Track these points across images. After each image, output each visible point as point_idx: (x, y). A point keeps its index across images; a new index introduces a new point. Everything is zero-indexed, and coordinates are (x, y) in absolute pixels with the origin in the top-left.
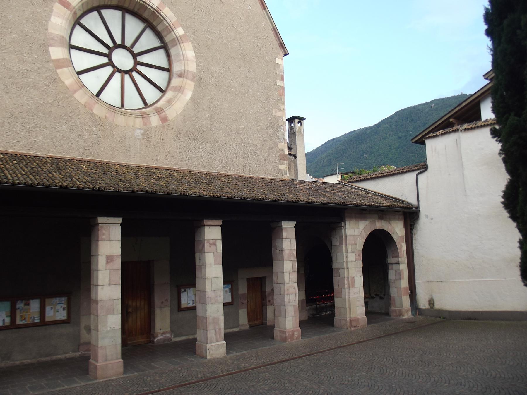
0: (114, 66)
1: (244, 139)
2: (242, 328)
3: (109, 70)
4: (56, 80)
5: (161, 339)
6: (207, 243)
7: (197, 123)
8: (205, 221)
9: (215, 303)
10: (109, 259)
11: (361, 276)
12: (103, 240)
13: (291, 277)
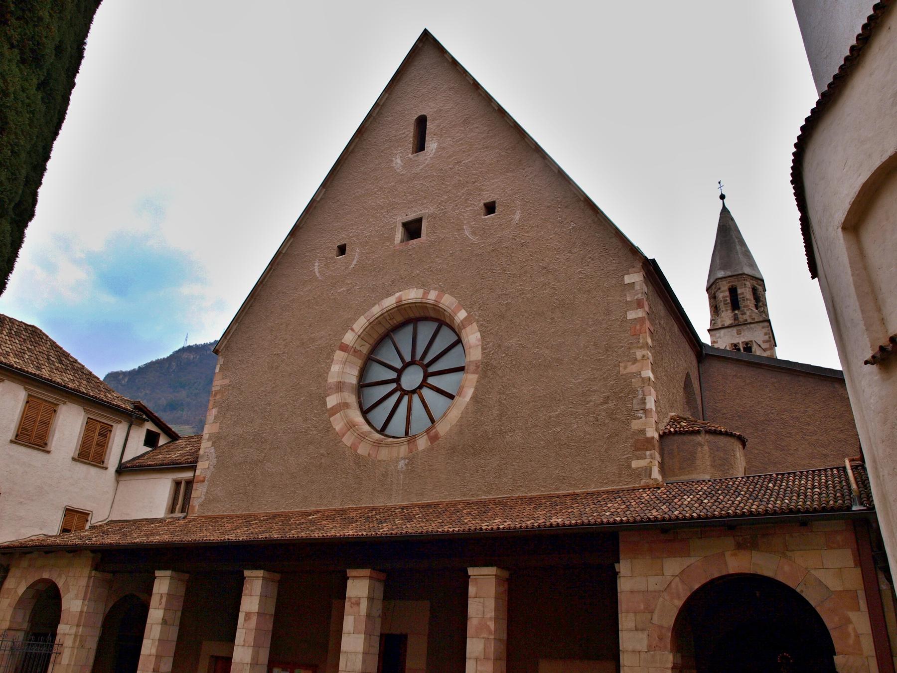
1: (558, 433)
4: (329, 428)
6: (348, 601)
7: (479, 429)
13: (479, 668)
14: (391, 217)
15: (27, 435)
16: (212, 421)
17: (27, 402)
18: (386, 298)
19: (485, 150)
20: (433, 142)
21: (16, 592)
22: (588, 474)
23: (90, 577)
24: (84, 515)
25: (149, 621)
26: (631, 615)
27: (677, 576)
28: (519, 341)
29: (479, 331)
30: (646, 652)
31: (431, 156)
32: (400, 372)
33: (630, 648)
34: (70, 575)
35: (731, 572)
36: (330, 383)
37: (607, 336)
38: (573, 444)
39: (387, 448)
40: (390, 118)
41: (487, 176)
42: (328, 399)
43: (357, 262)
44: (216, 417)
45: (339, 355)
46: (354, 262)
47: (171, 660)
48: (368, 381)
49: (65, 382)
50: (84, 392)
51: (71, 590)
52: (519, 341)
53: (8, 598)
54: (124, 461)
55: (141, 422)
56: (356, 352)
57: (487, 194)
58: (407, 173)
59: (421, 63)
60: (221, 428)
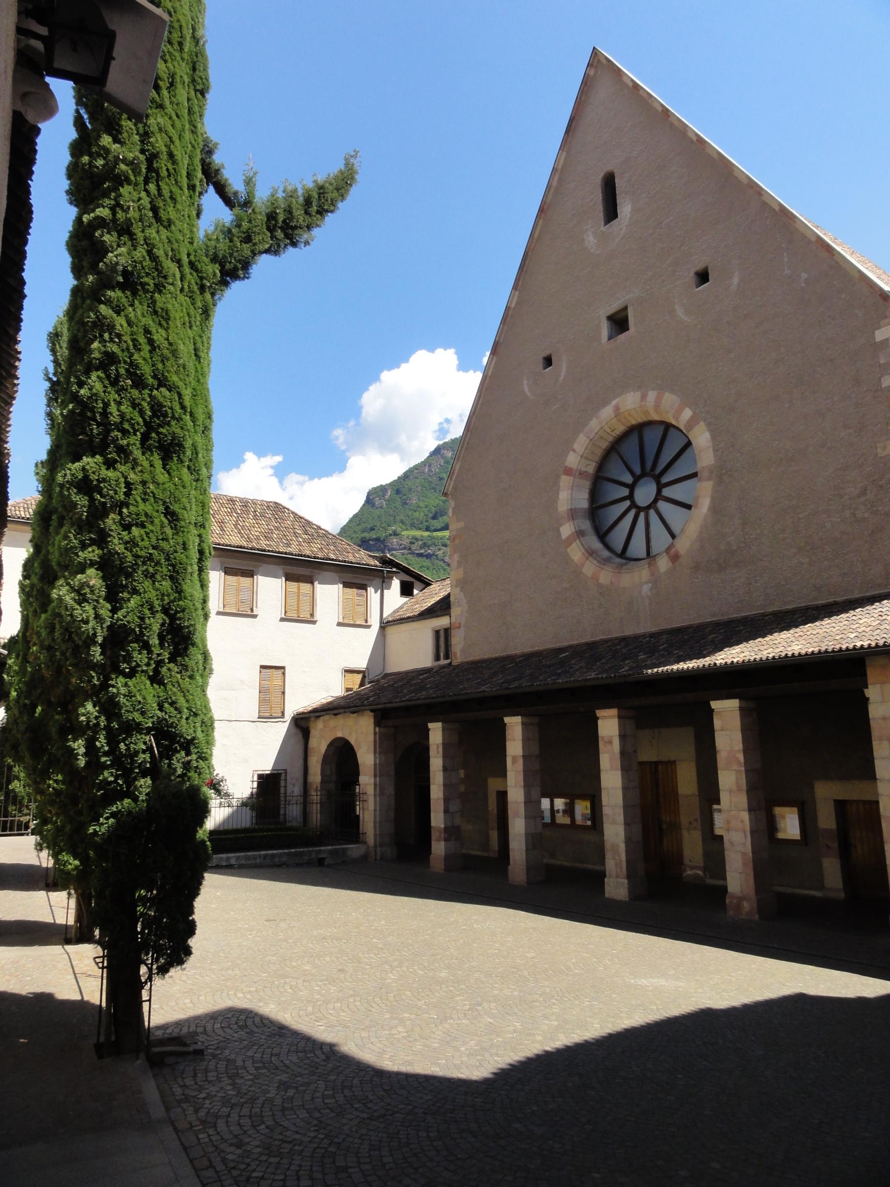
0: (655, 501)
3: (662, 505)
10: (514, 759)
25: (431, 769)
31: (626, 223)
42: (562, 529)
45: (565, 480)
46: (563, 373)
54: (385, 616)
56: (582, 474)
60: (465, 573)
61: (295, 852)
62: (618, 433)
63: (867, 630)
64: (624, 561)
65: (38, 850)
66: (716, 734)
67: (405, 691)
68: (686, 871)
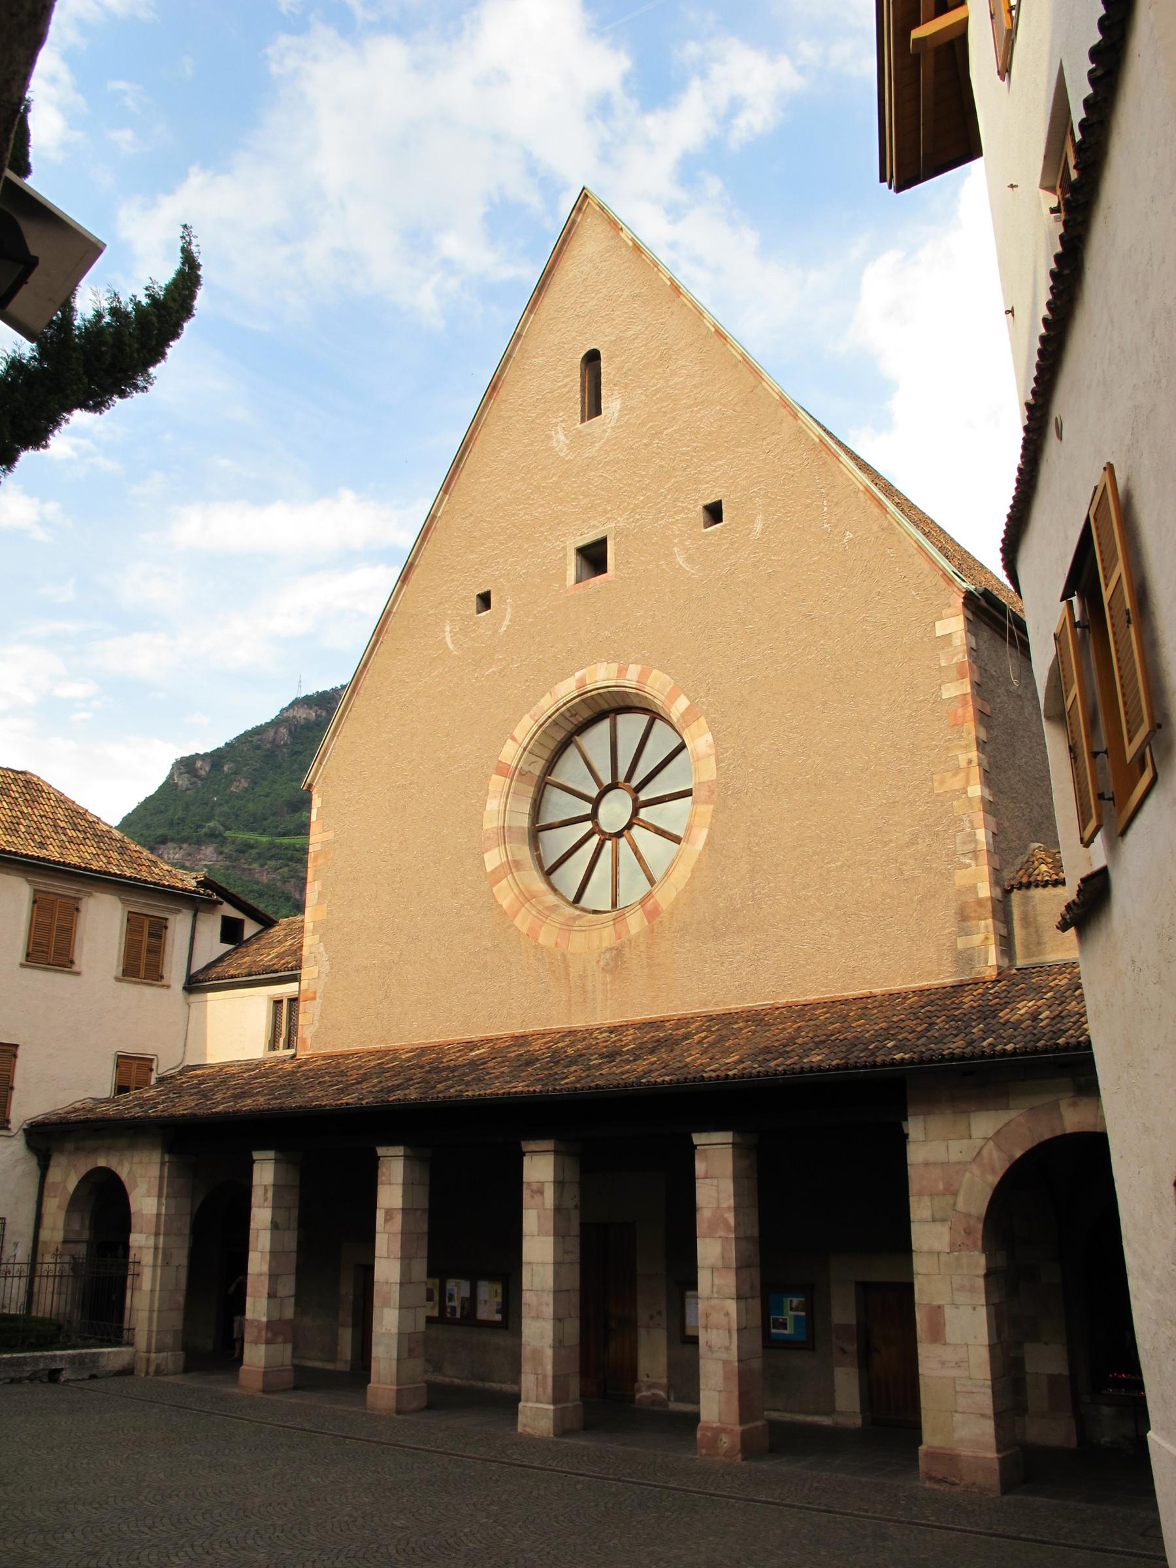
0: (629, 826)
2: (843, 1421)
4: (494, 905)
5: (647, 1397)
6: (527, 1189)
8: (523, 1143)
9: (538, 1317)
11: (979, 1308)
12: (383, 1184)
13: (716, 1281)
14: (557, 539)
15: (43, 952)
16: (315, 901)
17: (35, 902)
18: (561, 681)
19: (699, 407)
20: (614, 397)
21: (65, 1188)
22: (891, 962)
23: (163, 1164)
24: (145, 1063)
25: (253, 1225)
26: (926, 1200)
27: (991, 1138)
28: (774, 744)
29: (710, 730)
30: (948, 1253)
31: (612, 424)
32: (596, 803)
33: (925, 1248)
34: (134, 1161)
35: (1069, 1130)
36: (487, 830)
37: (912, 728)
38: (866, 914)
39: (583, 933)
40: (541, 359)
41: (706, 455)
42: (486, 856)
43: (510, 621)
44: (320, 894)
46: (506, 623)
47: (293, 1278)
48: (542, 823)
49: (86, 861)
50: (115, 873)
51: (139, 1183)
52: (774, 744)
53: (55, 1197)
55: (212, 905)
57: (707, 487)
58: (575, 457)
59: (582, 252)
61: (10, 1359)
62: (581, 719)
63: (910, 1037)
64: (578, 912)
65: (1025, 928)
66: (698, 1183)
67: (219, 1097)
68: (639, 1390)
